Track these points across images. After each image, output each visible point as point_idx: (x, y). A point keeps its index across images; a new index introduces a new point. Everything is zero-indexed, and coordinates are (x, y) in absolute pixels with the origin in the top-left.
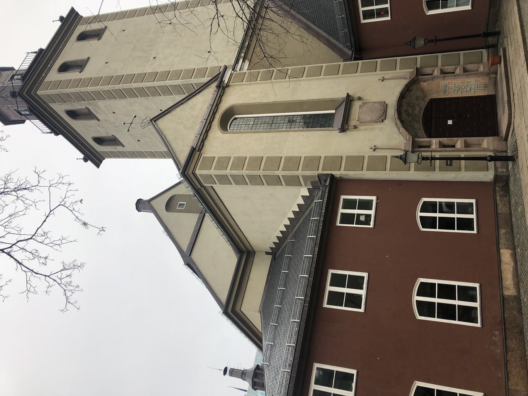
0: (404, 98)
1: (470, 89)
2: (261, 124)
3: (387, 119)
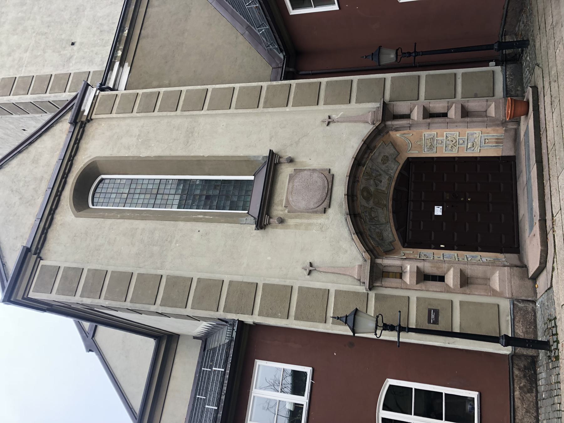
0: (361, 166)
1: (473, 144)
2: (140, 194)
3: (332, 206)
